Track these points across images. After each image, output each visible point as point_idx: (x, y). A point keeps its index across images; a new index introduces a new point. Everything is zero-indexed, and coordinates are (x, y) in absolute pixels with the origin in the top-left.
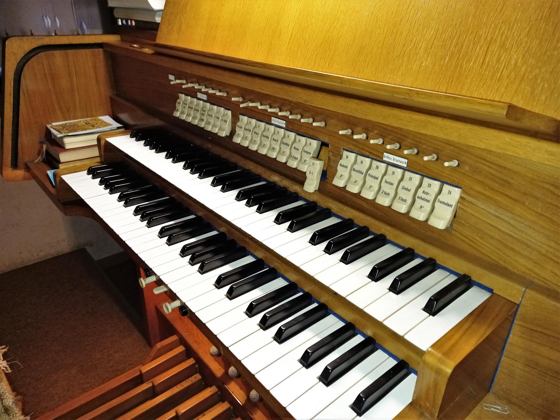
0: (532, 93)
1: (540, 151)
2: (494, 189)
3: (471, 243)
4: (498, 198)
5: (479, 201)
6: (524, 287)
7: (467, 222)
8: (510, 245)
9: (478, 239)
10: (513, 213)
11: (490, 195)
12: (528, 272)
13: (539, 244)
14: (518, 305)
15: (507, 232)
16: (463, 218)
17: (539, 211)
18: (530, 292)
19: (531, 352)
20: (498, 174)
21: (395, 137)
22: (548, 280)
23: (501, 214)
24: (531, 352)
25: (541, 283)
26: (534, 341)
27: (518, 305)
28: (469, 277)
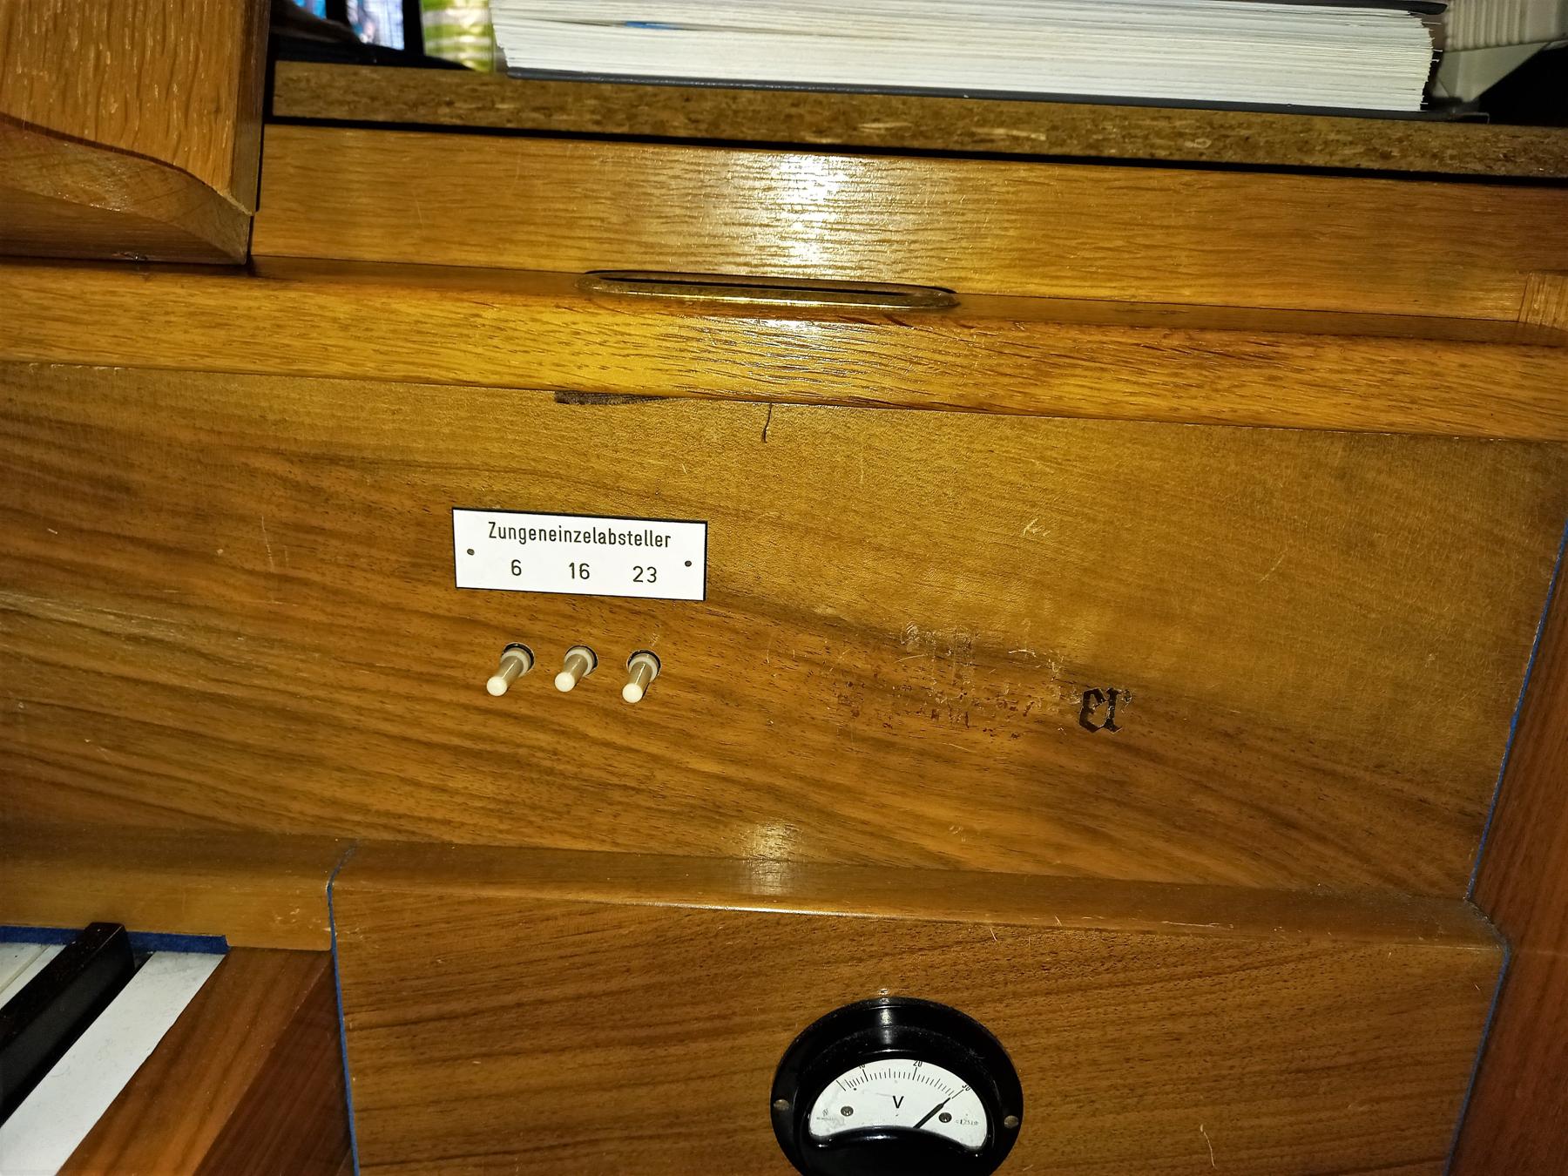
0: (63, 94)
1: (167, 318)
2: (81, 531)
3: (89, 783)
4: (115, 563)
5: (45, 595)
6: (323, 877)
7: (39, 703)
8: (233, 737)
9: (103, 753)
10: (189, 607)
11: (79, 558)
12: (328, 812)
13: (321, 693)
14: (330, 956)
15: (202, 689)
16: (18, 691)
17: (273, 569)
18: (348, 886)
19: (437, 1102)
20: (72, 464)
21: (880, 807)
22: (400, 817)
23: (148, 624)
24: (437, 1102)
25: (387, 836)
26: (431, 1061)
27: (330, 956)
28: (109, 927)
